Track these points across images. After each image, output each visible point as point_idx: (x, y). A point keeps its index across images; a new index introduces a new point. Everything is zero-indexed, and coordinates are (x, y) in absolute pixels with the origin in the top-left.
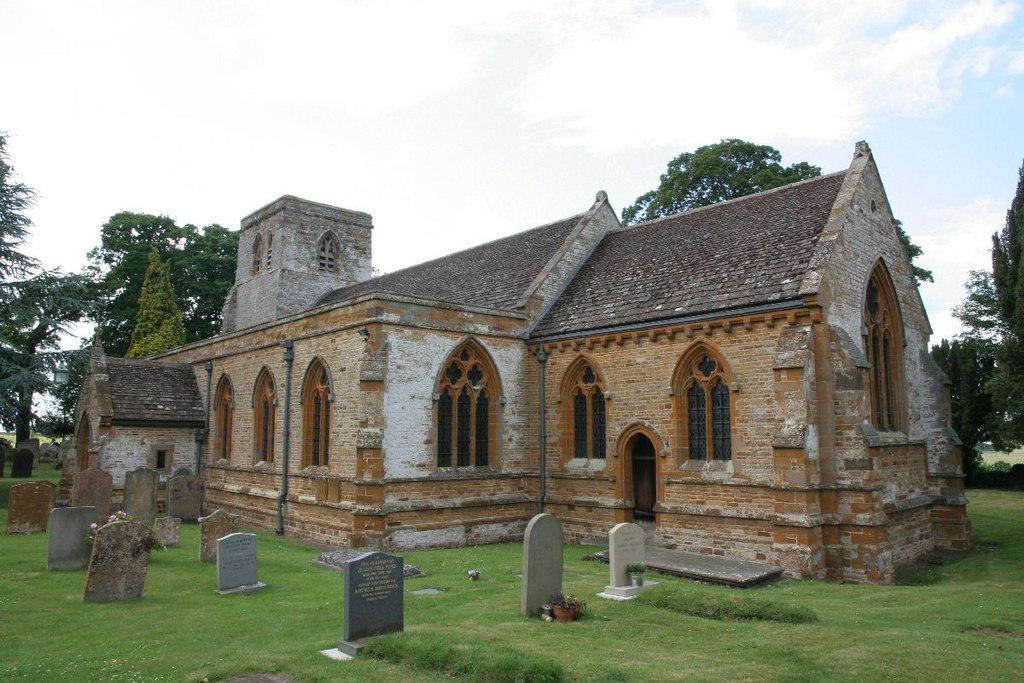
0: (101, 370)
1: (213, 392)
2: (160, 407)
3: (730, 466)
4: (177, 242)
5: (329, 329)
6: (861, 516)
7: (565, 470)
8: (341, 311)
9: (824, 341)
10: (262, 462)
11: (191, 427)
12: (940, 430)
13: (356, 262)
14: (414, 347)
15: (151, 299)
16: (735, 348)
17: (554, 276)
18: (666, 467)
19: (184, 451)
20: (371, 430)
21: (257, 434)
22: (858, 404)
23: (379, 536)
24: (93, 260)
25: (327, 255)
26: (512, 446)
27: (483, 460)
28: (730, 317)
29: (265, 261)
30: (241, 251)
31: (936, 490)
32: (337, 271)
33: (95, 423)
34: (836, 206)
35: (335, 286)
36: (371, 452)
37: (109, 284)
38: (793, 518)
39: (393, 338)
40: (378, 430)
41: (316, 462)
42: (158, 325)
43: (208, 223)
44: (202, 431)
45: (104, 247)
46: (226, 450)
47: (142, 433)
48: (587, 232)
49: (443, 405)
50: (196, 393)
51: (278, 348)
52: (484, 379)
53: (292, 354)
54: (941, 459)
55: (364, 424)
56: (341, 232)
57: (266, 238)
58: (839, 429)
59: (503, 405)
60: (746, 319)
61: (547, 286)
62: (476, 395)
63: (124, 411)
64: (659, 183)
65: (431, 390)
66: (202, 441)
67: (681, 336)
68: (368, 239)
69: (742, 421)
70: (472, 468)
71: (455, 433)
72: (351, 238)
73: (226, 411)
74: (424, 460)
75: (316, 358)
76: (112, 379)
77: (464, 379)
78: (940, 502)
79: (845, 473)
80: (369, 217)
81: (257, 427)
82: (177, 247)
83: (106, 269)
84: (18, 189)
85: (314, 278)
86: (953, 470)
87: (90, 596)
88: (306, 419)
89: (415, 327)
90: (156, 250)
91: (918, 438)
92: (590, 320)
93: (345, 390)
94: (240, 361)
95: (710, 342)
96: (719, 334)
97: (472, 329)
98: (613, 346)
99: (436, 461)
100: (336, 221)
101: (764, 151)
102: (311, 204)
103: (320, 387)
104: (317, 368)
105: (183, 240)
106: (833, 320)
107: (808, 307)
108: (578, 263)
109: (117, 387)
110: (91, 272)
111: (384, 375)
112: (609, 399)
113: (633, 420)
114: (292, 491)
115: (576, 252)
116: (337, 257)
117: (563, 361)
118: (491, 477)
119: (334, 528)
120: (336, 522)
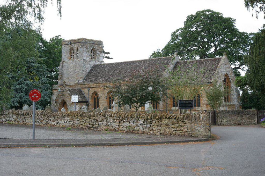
3: (200, 108)
7: (171, 109)
11: (86, 103)
25: (93, 54)
27: (156, 108)
32: (95, 59)
34: (219, 66)
70: (155, 109)
72: (98, 49)
80: (102, 42)
91: (233, 104)
100: (94, 44)
102: (89, 40)
116: (95, 54)
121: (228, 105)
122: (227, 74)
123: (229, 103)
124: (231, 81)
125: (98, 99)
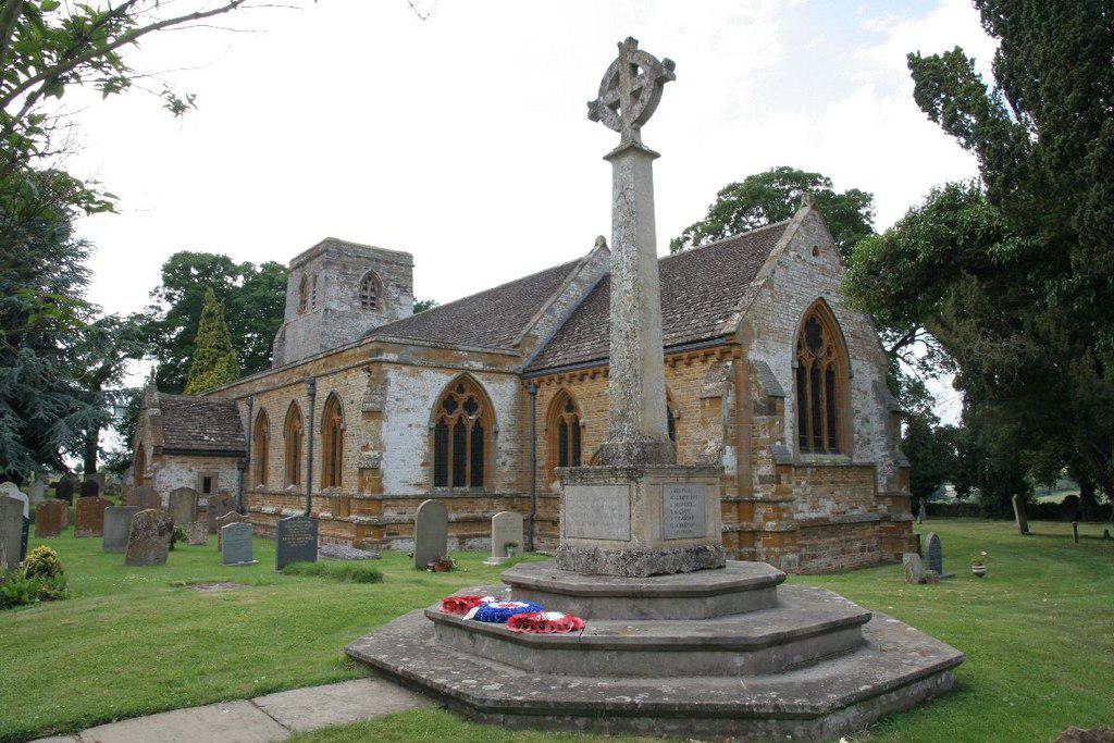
0: (154, 406)
1: (253, 424)
2: (206, 438)
4: (235, 280)
5: (342, 367)
6: (769, 523)
8: (351, 352)
9: (741, 373)
10: (292, 486)
12: (887, 453)
13: (397, 300)
15: (207, 339)
17: (549, 317)
19: (228, 478)
20: (371, 453)
21: (288, 462)
22: (770, 429)
23: (376, 543)
24: (155, 298)
26: (505, 469)
27: (478, 480)
28: (675, 353)
29: (310, 300)
30: (290, 290)
31: (883, 508)
32: (379, 309)
33: (149, 452)
35: (377, 324)
36: (371, 472)
37: (169, 323)
39: (392, 375)
40: (376, 453)
41: (333, 484)
42: (214, 363)
43: (267, 260)
44: (244, 460)
45: (165, 286)
46: (263, 478)
48: (584, 274)
50: (239, 427)
51: (303, 385)
52: (480, 410)
53: (314, 388)
54: (889, 480)
55: (366, 448)
56: (382, 273)
57: (310, 279)
58: (754, 450)
59: (496, 432)
61: (543, 326)
62: (471, 425)
63: (175, 441)
65: (427, 419)
66: (244, 469)
68: (409, 277)
69: (684, 444)
73: (263, 440)
75: (332, 393)
76: (164, 411)
77: (460, 410)
78: (886, 518)
79: (758, 487)
80: (411, 257)
81: (288, 454)
82: (235, 284)
83: (167, 307)
84: (82, 243)
85: (357, 317)
86: (897, 490)
87: (129, 562)
88: (325, 445)
89: (412, 365)
90: (211, 290)
91: (865, 461)
92: (571, 357)
93: (353, 419)
94: (275, 396)
97: (467, 365)
98: (587, 380)
99: (432, 480)
101: (814, 179)
102: (353, 246)
103: (336, 417)
104: (333, 399)
105: (241, 278)
106: (754, 355)
107: (729, 346)
108: (573, 304)
109: (165, 418)
110: (152, 311)
111: (382, 406)
112: (584, 427)
114: (314, 510)
115: (573, 293)
117: (548, 393)
118: (485, 497)
119: (344, 538)
120: (346, 534)
121: (835, 467)
122: (821, 298)
123: (841, 459)
124: (850, 340)
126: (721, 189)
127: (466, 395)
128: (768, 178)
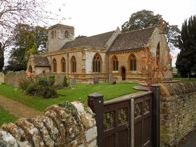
0: (33, 58)
1: (52, 61)
14: (89, 54)
16: (137, 54)
18: (127, 72)
19: (47, 70)
27: (99, 71)
29: (54, 36)
32: (68, 38)
33: (33, 67)
36: (84, 70)
38: (143, 78)
39: (86, 53)
41: (73, 72)
47: (41, 68)
48: (116, 34)
49: (93, 63)
55: (83, 66)
56: (69, 31)
57: (54, 32)
60: (139, 50)
61: (109, 43)
64: (129, 19)
66: (50, 69)
67: (129, 52)
71: (95, 67)
73: (55, 65)
74: (91, 71)
77: (96, 59)
85: (64, 39)
93: (78, 61)
95: (134, 53)
96: (135, 52)
98: (119, 54)
104: (73, 58)
108: (114, 39)
113: (122, 65)
115: (114, 37)
117: (111, 56)
125: (76, 63)
126: (132, 14)
127: (97, 56)
128: (141, 12)
